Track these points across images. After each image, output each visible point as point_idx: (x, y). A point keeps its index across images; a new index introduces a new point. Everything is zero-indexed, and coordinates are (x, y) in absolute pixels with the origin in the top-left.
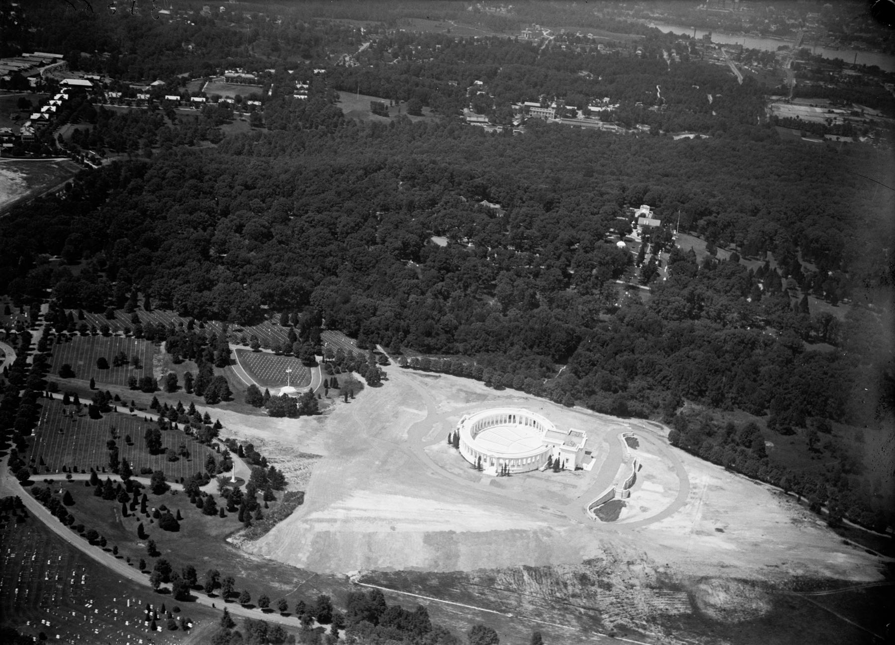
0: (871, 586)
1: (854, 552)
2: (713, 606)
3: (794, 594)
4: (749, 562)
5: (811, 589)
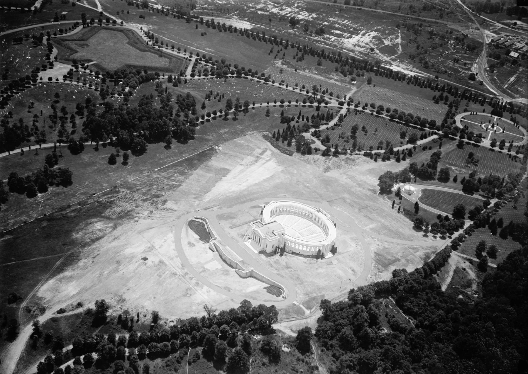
0: (40, 284)
1: (69, 302)
2: (97, 222)
3: (71, 251)
4: (108, 250)
5: (66, 259)
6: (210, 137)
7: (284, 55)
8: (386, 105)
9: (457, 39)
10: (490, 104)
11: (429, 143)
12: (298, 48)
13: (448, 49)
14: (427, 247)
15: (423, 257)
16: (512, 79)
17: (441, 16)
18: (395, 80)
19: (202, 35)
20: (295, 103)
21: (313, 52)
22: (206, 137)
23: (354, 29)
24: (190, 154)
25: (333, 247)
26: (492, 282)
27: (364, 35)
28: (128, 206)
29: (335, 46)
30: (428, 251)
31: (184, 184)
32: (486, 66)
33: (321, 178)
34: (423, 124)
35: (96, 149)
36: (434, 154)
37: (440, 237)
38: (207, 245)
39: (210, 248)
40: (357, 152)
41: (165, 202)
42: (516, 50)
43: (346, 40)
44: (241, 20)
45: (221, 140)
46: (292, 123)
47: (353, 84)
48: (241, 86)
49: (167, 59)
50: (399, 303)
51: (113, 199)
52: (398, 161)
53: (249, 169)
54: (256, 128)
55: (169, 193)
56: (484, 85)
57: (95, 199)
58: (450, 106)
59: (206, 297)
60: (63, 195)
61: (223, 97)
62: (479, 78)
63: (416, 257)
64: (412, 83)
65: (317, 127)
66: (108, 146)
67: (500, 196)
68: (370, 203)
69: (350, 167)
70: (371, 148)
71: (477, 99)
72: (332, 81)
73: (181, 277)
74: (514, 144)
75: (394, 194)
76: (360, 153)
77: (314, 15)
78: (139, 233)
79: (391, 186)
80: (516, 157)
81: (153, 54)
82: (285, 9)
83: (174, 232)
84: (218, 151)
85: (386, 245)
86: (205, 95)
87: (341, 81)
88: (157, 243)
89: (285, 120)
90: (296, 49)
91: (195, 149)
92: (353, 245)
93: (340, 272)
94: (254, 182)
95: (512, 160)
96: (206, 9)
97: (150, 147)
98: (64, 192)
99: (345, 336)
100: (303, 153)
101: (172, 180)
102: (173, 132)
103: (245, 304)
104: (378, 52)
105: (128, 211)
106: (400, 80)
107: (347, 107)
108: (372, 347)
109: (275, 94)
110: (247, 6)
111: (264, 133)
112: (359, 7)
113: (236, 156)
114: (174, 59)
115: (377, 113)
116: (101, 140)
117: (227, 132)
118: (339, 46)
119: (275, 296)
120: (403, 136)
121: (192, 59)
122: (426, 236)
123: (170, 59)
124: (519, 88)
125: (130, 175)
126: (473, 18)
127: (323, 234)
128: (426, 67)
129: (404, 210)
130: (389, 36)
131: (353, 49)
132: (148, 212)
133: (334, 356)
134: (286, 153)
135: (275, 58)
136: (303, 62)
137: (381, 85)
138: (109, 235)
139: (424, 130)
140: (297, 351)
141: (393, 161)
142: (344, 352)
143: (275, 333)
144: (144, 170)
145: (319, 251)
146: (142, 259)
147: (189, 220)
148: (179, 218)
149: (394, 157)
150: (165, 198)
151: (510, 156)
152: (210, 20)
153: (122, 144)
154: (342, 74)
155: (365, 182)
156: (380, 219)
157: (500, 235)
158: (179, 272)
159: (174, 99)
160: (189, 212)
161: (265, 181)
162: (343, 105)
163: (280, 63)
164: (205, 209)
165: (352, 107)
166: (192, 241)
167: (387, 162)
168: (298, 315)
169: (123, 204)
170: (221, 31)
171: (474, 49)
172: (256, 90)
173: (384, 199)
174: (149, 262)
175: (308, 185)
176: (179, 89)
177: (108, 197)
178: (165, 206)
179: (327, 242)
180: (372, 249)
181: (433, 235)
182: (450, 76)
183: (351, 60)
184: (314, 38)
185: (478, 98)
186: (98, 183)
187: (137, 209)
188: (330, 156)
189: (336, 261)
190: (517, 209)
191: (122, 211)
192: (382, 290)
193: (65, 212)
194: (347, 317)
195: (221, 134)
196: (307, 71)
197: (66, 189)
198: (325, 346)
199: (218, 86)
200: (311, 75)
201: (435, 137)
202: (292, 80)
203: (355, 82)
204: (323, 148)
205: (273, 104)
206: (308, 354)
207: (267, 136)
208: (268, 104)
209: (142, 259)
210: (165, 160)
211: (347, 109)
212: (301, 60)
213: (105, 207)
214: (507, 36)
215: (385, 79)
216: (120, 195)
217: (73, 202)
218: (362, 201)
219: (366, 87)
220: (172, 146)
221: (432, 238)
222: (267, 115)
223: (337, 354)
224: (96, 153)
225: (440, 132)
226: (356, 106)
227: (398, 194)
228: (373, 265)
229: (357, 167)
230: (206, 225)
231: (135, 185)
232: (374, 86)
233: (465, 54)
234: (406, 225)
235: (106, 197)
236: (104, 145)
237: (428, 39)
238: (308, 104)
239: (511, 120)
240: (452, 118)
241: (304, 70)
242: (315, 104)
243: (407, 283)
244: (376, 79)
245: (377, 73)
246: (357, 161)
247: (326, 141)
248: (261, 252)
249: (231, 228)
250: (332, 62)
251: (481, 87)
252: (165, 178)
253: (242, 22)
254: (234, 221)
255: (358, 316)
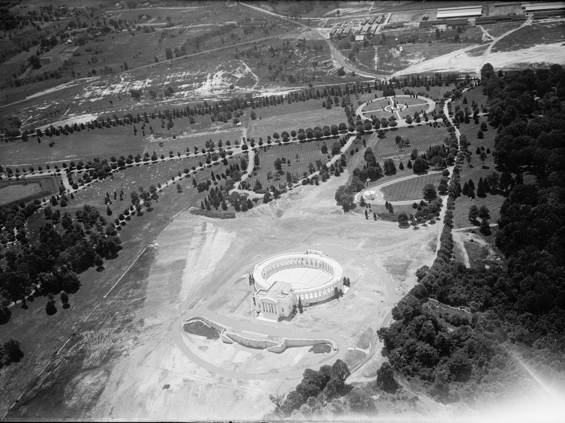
2: (83, 378)
6: (138, 239)
7: (151, 128)
8: (289, 130)
9: (299, 46)
10: (376, 88)
11: (351, 146)
12: (160, 116)
13: (299, 58)
14: (425, 237)
15: (430, 248)
16: (376, 59)
17: (266, 33)
18: (275, 105)
19: (51, 146)
20: (199, 168)
21: (177, 114)
22: (134, 240)
23: (198, 76)
24: (130, 265)
25: (345, 279)
26: (506, 239)
27: (211, 78)
28: (105, 346)
29: (193, 99)
30: (429, 241)
31: (148, 296)
32: (344, 58)
33: (280, 224)
34: (335, 131)
35: (25, 307)
36: (367, 153)
37: (429, 223)
38: (220, 340)
39: (224, 342)
40: (294, 185)
41: (142, 322)
42: (359, 33)
43: (199, 90)
44: (80, 115)
45: (150, 237)
46: (212, 186)
47: (239, 126)
48: (133, 176)
49: (34, 185)
50: (443, 299)
51: (81, 348)
52: (337, 175)
53: (203, 250)
54: (177, 209)
55: (138, 311)
56: (357, 75)
57: (62, 357)
58: (344, 105)
59: (259, 390)
60: (22, 371)
61: (123, 194)
62: (347, 70)
63: (424, 251)
64: (293, 101)
65: (238, 179)
66: (35, 299)
67: (451, 162)
68: (343, 224)
69: (299, 201)
70: (305, 175)
71: (362, 88)
72: (217, 132)
73: (218, 385)
74: (427, 112)
75: (358, 205)
76: (298, 184)
77: (148, 81)
78: (140, 364)
79: (352, 199)
80: (436, 123)
81: (16, 186)
82: (115, 87)
83: (176, 345)
84: (156, 248)
85: (388, 254)
86: (103, 201)
87: (226, 128)
88: (167, 364)
89: (202, 188)
90: (157, 118)
91: (131, 258)
92: (359, 269)
93: (368, 299)
94: (219, 259)
95: (435, 127)
96: (33, 120)
97: (82, 277)
98: (21, 367)
99: (424, 352)
100: (245, 210)
101: (131, 298)
102: (97, 250)
103: (309, 373)
104: (237, 87)
105: (109, 350)
106: (279, 103)
107: (252, 148)
108: (453, 350)
109: (172, 168)
110: (74, 100)
111: (190, 209)
112: (184, 57)
113: (180, 244)
114: (42, 181)
115: (284, 141)
116: (26, 294)
117: (151, 225)
118: (197, 98)
119: (325, 353)
120: (324, 150)
121: (60, 172)
122: (416, 228)
123: (38, 182)
124: (389, 64)
125: (81, 315)
126: (297, 23)
127: (324, 274)
128: (292, 81)
129: (379, 216)
130: (236, 69)
131: (212, 94)
132: (131, 340)
133: (423, 378)
134: (228, 218)
135: (144, 135)
136: (175, 126)
137: (266, 115)
138: (109, 383)
139: (338, 137)
140: (385, 393)
141: (333, 177)
142: (431, 369)
143: (353, 388)
144: (93, 303)
145: (336, 289)
146: (163, 388)
147: (183, 325)
148: (170, 329)
149: (332, 173)
150: (139, 319)
151: (431, 124)
152: (49, 129)
153: (49, 289)
154: (222, 121)
155: (323, 208)
156: (364, 234)
157: (478, 195)
158: (211, 380)
159: (73, 219)
160: (176, 319)
161: (229, 252)
162: (247, 148)
163: (153, 138)
164: (191, 307)
165: (257, 146)
166: (202, 344)
167: (329, 180)
168: (361, 359)
169: (97, 346)
170: (67, 134)
171: (321, 48)
172: (150, 173)
173: (353, 214)
174: (173, 387)
175: (272, 236)
176: (71, 207)
177: (75, 348)
178: (145, 326)
179: (338, 277)
180: (379, 264)
181: (422, 224)
182: (319, 80)
183: (220, 105)
184: (166, 100)
185: (361, 88)
186: (52, 340)
187: (115, 344)
188: (271, 200)
189: (356, 291)
190: (473, 167)
191: (102, 354)
192: (422, 293)
193: (37, 387)
194: (410, 334)
195: (146, 231)
196: (185, 133)
197: (20, 364)
198: (409, 374)
199: (110, 186)
200: (193, 135)
201: (352, 139)
202: (176, 148)
203: (240, 123)
204: (261, 196)
205: (178, 178)
206: (398, 390)
207: (194, 210)
208: (173, 179)
209: (163, 388)
210: (108, 283)
211: (253, 150)
212: (171, 127)
213: (80, 359)
214: (340, 25)
215: (265, 109)
216: (85, 339)
217: (38, 372)
218: (335, 226)
219: (254, 123)
220: (105, 266)
221: (424, 227)
222: (180, 192)
223: (427, 374)
224: (26, 311)
225: (355, 132)
226: (261, 143)
227: (363, 204)
228: (391, 278)
229: (305, 198)
230: (203, 322)
231: (94, 322)
232: (261, 119)
233: (317, 55)
234: (392, 228)
235: (71, 349)
236: (31, 299)
237: (272, 57)
238: (213, 162)
239: (406, 94)
240: (354, 115)
241: (181, 133)
242: (220, 159)
243: (437, 277)
244: (257, 111)
245: (253, 106)
246: (301, 192)
247: (258, 188)
248: (281, 319)
249: (232, 312)
250: (203, 115)
251: (355, 78)
252: (122, 299)
253: (81, 116)
254: (230, 304)
255: (423, 327)
